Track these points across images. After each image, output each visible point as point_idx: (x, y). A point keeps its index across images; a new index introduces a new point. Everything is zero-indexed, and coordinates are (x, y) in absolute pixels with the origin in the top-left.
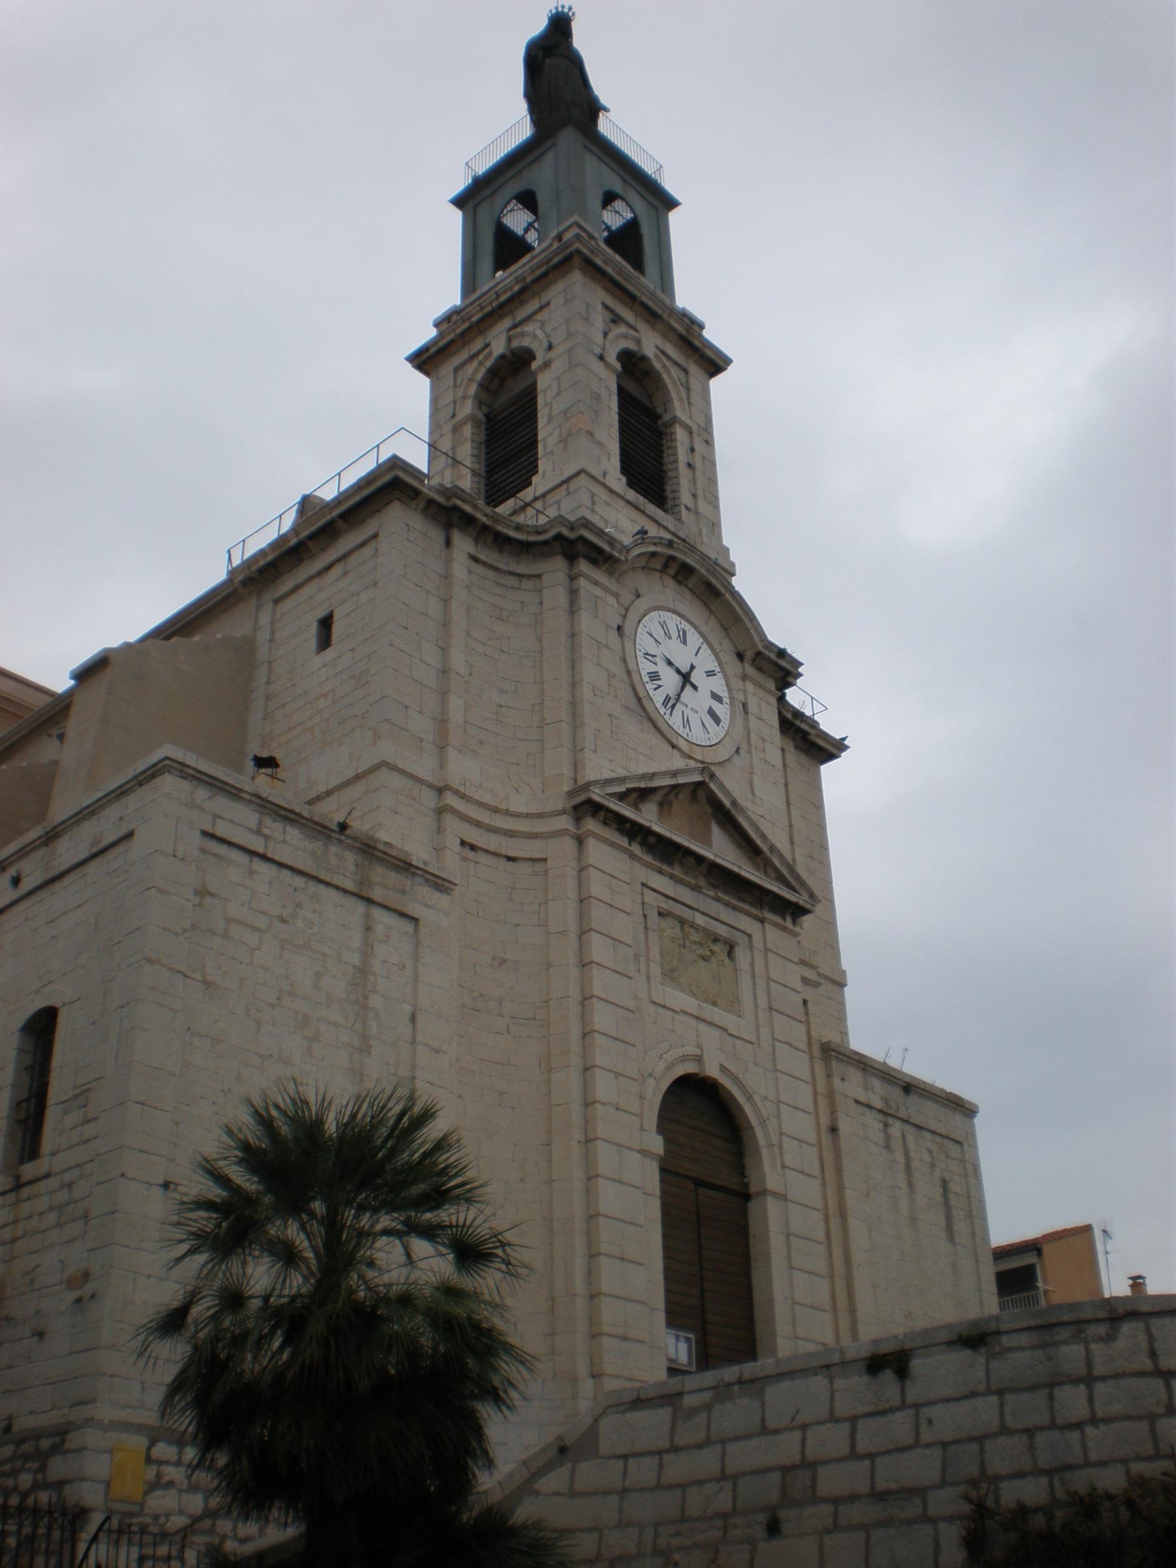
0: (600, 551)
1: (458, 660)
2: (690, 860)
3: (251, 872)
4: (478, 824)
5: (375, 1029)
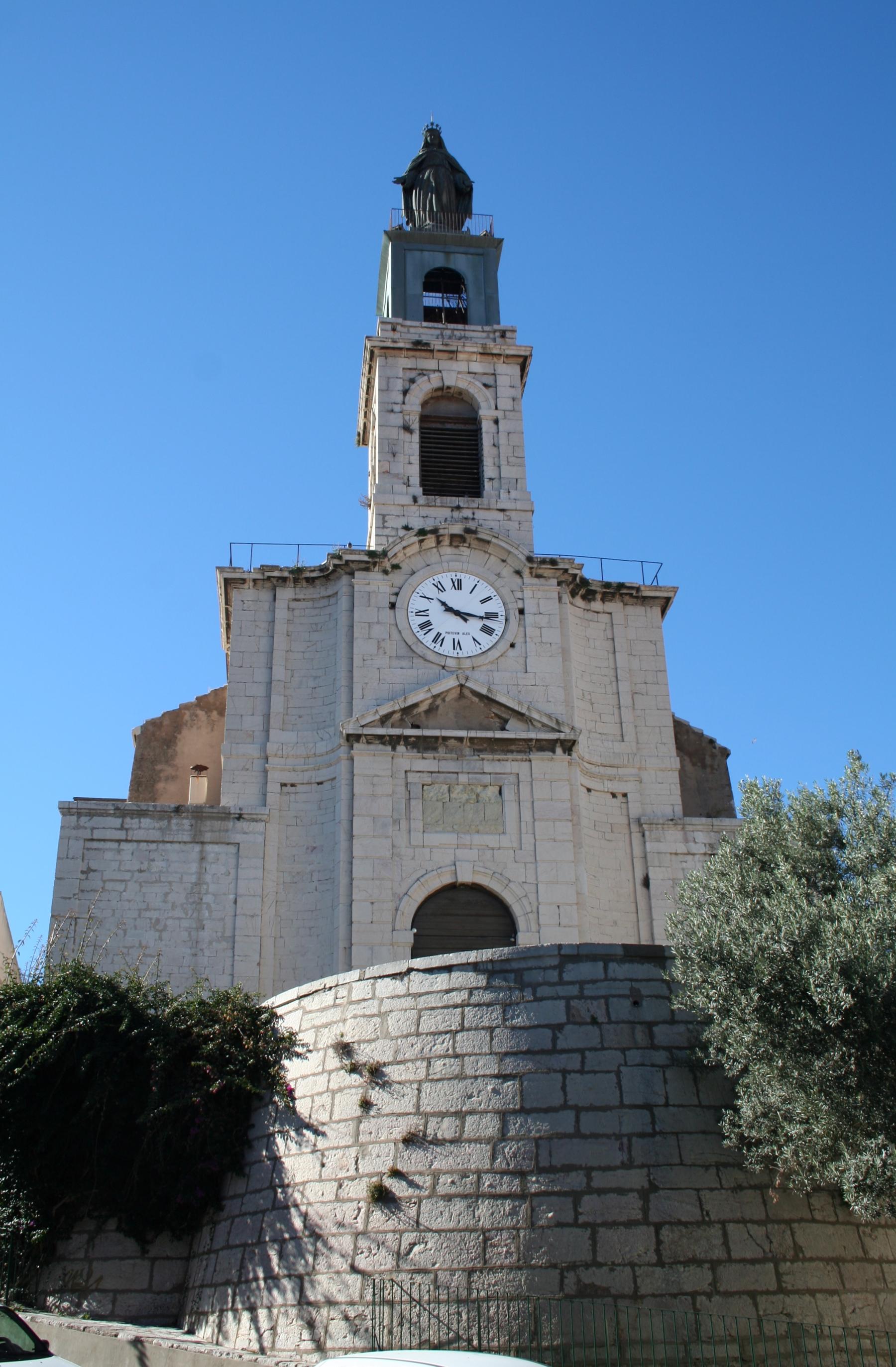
1: (279, 672)
3: (119, 851)
5: (207, 914)
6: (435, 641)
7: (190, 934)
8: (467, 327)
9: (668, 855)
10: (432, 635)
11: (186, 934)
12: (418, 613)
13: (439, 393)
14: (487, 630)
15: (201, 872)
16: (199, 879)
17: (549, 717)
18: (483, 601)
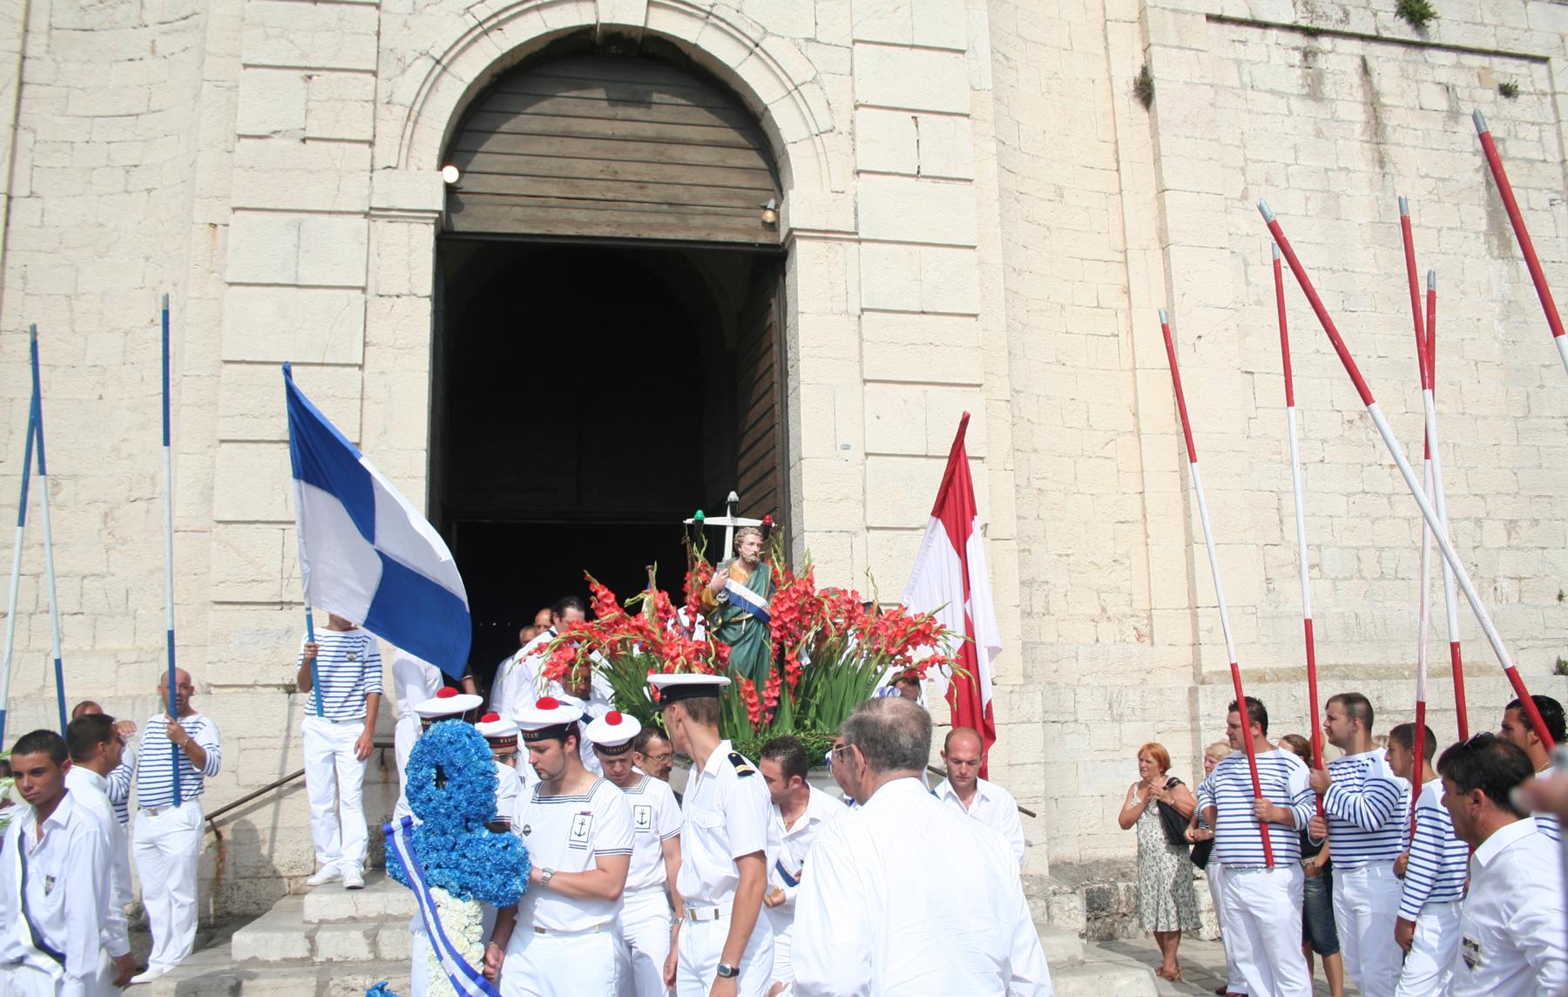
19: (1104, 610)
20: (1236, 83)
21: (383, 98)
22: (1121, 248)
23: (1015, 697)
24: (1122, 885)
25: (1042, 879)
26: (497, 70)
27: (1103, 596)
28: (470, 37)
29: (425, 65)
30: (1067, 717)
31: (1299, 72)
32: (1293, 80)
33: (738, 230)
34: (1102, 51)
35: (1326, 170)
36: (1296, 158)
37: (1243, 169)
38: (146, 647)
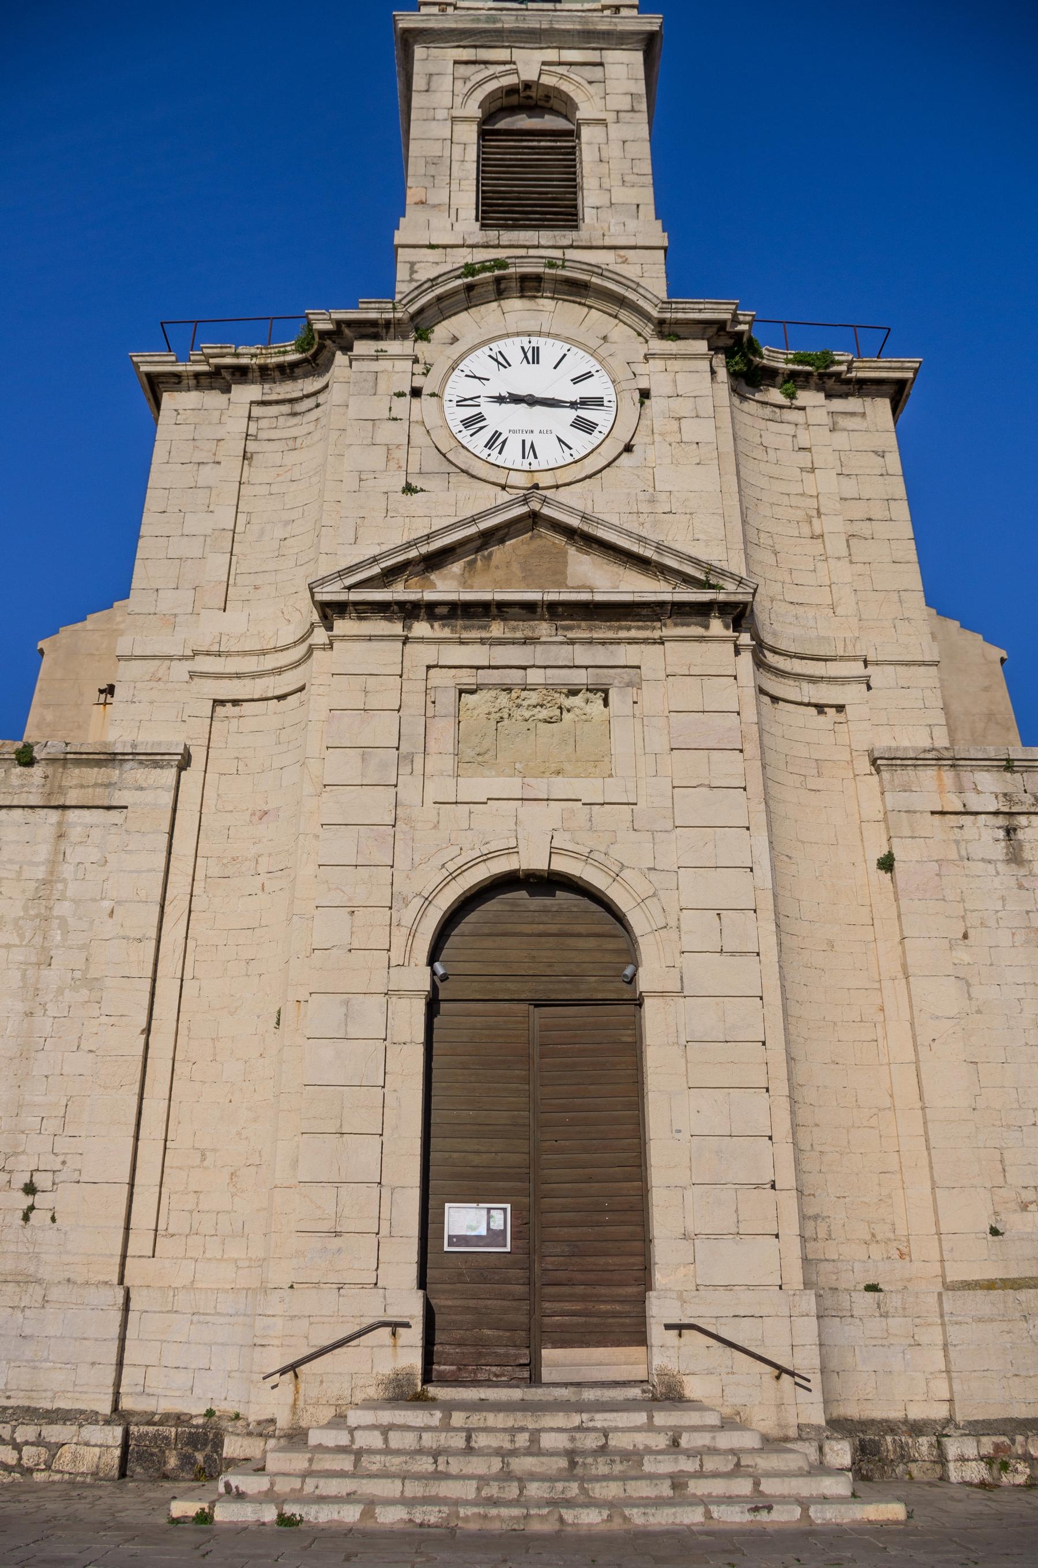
0: (373, 323)
2: (517, 610)
4: (218, 676)
5: (59, 938)
6: (489, 445)
7: (24, 976)
8: (559, 6)
9: (760, 923)
10: (485, 435)
11: (18, 975)
12: (461, 403)
13: (514, 100)
14: (585, 426)
15: (57, 858)
16: (52, 873)
17: (696, 562)
18: (576, 381)
19: (873, 1235)
20: (956, 857)
21: (394, 922)
22: (877, 978)
23: (797, 1298)
24: (889, 1439)
25: (819, 1427)
26: (462, 899)
27: (872, 1226)
28: (445, 882)
29: (418, 902)
30: (845, 1314)
31: (1003, 844)
32: (999, 851)
33: (610, 991)
34: (859, 843)
35: (1028, 912)
36: (1004, 906)
37: (963, 917)
38: (254, 1257)
